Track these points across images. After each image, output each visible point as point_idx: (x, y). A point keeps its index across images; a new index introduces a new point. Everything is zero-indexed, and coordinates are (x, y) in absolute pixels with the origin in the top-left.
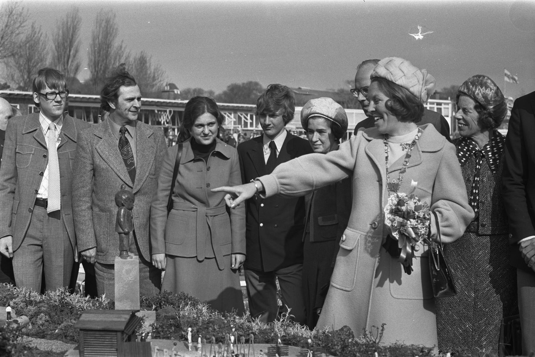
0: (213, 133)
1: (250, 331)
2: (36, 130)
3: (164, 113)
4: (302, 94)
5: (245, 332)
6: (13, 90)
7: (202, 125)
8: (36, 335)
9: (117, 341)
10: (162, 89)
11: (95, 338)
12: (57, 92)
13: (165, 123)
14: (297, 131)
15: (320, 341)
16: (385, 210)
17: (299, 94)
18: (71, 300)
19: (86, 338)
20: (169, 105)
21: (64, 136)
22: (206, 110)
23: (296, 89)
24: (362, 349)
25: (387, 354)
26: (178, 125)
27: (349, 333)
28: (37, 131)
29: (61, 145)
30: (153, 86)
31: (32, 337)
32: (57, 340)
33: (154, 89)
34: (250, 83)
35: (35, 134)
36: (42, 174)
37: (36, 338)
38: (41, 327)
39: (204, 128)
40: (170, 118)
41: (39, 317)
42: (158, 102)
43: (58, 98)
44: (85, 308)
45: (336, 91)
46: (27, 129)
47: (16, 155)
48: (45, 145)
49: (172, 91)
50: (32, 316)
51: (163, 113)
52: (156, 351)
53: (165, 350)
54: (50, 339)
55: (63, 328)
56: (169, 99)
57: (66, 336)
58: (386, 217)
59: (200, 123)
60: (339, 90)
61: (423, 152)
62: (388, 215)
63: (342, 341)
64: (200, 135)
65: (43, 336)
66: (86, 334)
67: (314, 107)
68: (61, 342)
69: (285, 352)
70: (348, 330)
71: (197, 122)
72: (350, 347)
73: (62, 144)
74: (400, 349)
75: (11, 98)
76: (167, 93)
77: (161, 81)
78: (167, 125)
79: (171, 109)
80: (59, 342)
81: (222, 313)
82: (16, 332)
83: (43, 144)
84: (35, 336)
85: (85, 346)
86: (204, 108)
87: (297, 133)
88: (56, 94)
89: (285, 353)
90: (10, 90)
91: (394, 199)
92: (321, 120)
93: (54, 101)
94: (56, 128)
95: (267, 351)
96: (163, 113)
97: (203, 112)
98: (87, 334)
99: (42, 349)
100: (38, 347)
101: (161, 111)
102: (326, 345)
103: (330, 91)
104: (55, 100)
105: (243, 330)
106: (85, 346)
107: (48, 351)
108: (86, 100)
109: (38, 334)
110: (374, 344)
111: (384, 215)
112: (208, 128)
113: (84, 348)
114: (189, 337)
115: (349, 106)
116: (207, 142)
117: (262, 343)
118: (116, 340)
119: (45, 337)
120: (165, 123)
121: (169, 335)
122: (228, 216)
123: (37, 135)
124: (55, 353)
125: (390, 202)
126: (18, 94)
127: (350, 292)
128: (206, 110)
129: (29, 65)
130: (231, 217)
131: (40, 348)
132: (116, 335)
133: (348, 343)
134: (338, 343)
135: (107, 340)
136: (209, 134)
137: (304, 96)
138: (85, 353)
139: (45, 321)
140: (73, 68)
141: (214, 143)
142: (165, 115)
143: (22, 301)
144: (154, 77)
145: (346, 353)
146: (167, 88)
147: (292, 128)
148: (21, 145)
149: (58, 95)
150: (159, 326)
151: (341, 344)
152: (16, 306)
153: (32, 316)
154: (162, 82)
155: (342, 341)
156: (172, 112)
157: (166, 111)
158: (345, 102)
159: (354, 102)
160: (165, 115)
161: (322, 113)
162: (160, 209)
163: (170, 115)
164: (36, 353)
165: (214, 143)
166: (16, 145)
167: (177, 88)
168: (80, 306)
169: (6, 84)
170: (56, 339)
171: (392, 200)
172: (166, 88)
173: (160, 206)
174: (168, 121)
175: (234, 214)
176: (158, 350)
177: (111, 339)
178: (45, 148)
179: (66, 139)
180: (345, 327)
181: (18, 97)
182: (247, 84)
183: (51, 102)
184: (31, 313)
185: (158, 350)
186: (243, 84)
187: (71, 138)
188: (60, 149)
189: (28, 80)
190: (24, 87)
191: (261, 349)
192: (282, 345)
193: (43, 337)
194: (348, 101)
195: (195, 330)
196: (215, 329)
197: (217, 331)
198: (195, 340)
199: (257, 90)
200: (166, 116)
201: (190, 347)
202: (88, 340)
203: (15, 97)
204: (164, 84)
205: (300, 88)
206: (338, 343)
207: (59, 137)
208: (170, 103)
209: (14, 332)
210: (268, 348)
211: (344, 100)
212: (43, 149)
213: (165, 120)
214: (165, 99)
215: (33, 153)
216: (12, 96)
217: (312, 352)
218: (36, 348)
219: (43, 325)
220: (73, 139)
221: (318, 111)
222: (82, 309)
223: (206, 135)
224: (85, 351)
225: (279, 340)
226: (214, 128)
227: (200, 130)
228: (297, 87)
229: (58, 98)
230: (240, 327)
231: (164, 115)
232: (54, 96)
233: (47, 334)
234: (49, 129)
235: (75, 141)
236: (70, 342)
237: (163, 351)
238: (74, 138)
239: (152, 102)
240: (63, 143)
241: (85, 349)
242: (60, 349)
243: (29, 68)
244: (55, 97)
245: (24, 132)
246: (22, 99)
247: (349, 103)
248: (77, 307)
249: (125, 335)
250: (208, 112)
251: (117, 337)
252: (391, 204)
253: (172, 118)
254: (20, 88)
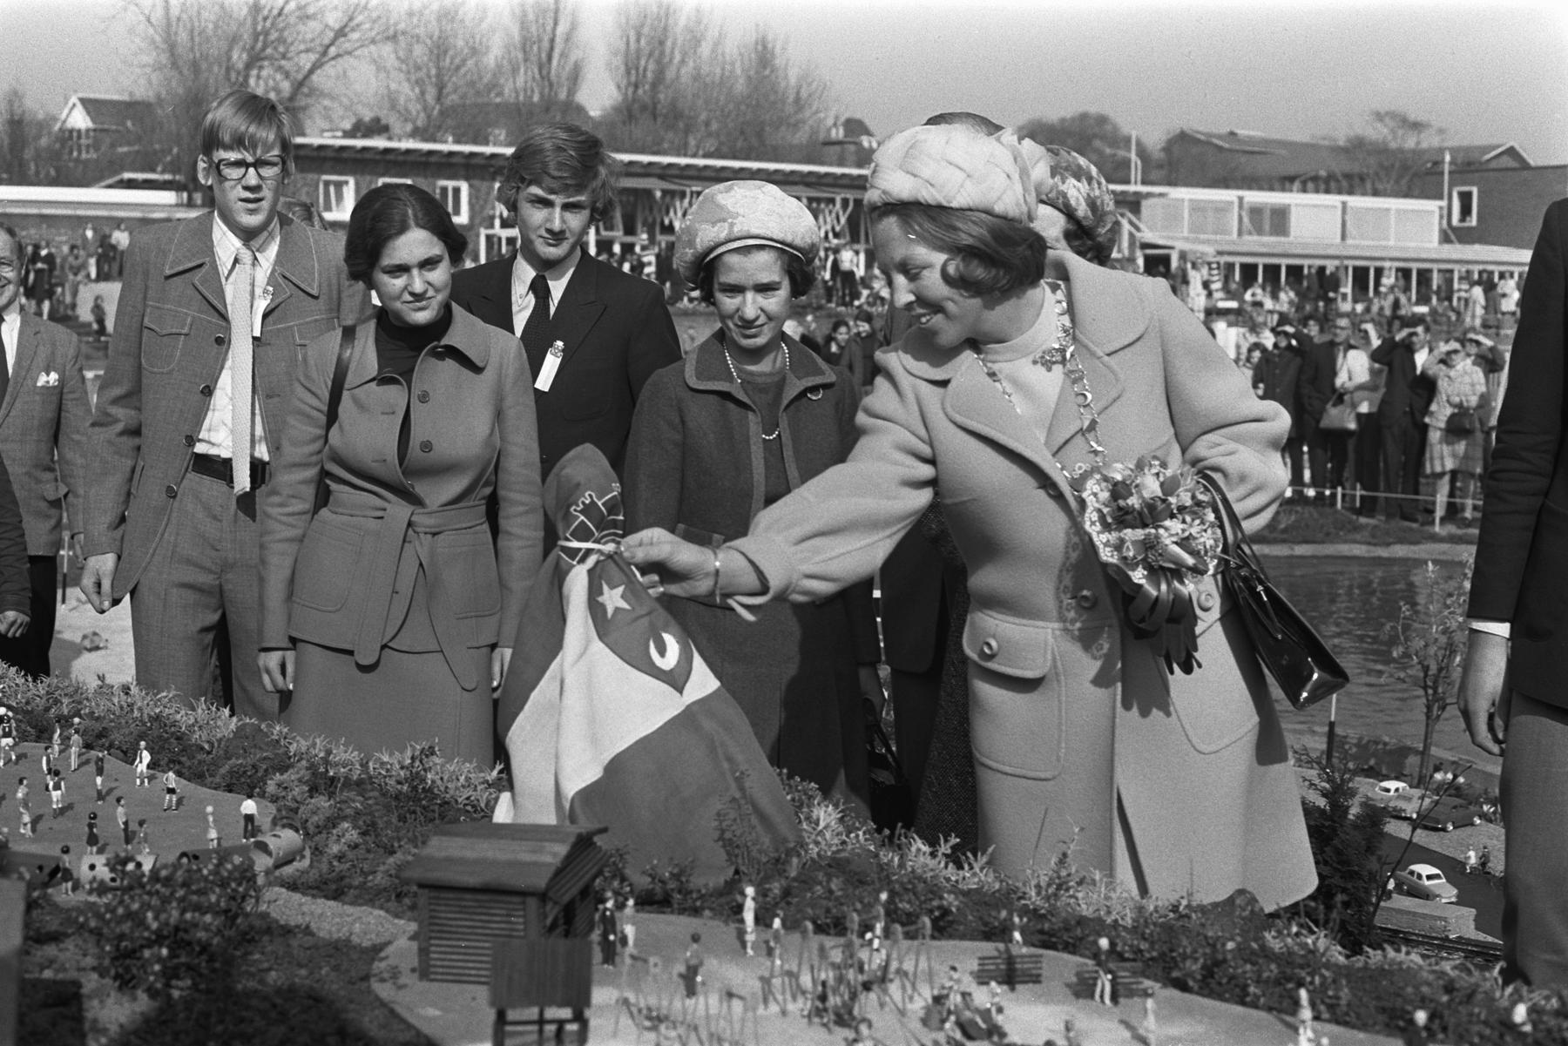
0: (437, 290)
1: (935, 903)
2: (200, 266)
3: (827, 205)
4: (1237, 151)
5: (921, 903)
6: (400, 140)
7: (403, 269)
8: (317, 888)
9: (524, 923)
10: (822, 137)
11: (460, 912)
12: (250, 159)
13: (831, 235)
14: (1218, 263)
15: (1145, 939)
16: (1087, 526)
17: (1230, 150)
18: (442, 779)
19: (434, 910)
20: (825, 181)
21: (280, 280)
22: (412, 223)
23: (1220, 137)
24: (1265, 975)
25: (1342, 994)
26: (867, 241)
27: (1252, 911)
28: (204, 270)
29: (273, 306)
30: (796, 126)
31: (304, 894)
32: (373, 906)
33: (801, 137)
34: (1084, 117)
35: (197, 277)
36: (208, 392)
37: (314, 896)
38: (335, 863)
39: (411, 277)
40: (843, 220)
41: (335, 831)
42: (810, 173)
43: (252, 178)
44: (483, 805)
45: (1341, 143)
46: (174, 263)
47: (141, 331)
48: (223, 311)
49: (850, 143)
50: (318, 827)
51: (823, 206)
52: (628, 961)
53: (652, 960)
54: (352, 904)
55: (393, 872)
56: (841, 164)
57: (399, 896)
58: (1098, 543)
59: (397, 262)
60: (1349, 140)
61: (1108, 355)
62: (1101, 538)
63: (1209, 944)
64: (399, 297)
65: (336, 890)
66: (434, 898)
67: (740, 218)
68: (382, 913)
69: (1034, 972)
70: (1247, 905)
71: (387, 260)
72: (1232, 964)
73: (277, 301)
74: (1391, 972)
75: (389, 162)
76: (837, 148)
77: (817, 112)
78: (835, 241)
79: (848, 196)
80: (377, 912)
81: (887, 832)
82: (240, 884)
83: (220, 307)
84: (315, 892)
85: (433, 935)
86: (405, 215)
87: (1218, 268)
88: (248, 166)
89: (1031, 975)
90: (390, 139)
91: (1096, 489)
92: (764, 257)
93: (239, 187)
94: (256, 258)
95: (975, 967)
96: (823, 206)
97: (403, 229)
98: (438, 898)
99: (321, 934)
100: (313, 926)
101: (818, 200)
102: (1163, 955)
103: (1322, 142)
104: (244, 182)
105: (918, 898)
106: (433, 935)
107: (338, 940)
108: (639, 170)
109: (325, 883)
110: (1310, 956)
111: (1091, 539)
112: (420, 274)
113: (431, 938)
114: (749, 916)
115: (1380, 187)
116: (422, 317)
117: (970, 939)
118: (521, 920)
119: (343, 893)
120: (831, 235)
121: (698, 903)
122: (489, 535)
123: (204, 281)
124: (355, 947)
125: (1091, 502)
126: (408, 151)
127: (1052, 783)
128: (412, 223)
129: (438, 68)
130: (500, 543)
131: (319, 928)
132: (524, 903)
133: (1225, 952)
134: (1195, 951)
135: (498, 919)
136: (426, 292)
137: (1243, 159)
138: (433, 956)
139: (349, 846)
140: (564, 75)
141: (443, 322)
142: (830, 212)
143: (300, 780)
144: (797, 99)
145: (1220, 984)
146: (838, 133)
147: (1202, 253)
148: (158, 308)
149: (251, 170)
150: (671, 873)
151: (1205, 954)
152: (284, 794)
153: (318, 827)
154: (822, 115)
155: (1209, 944)
156: (851, 204)
157: (832, 201)
158: (1368, 175)
159: (1394, 175)
160: (830, 212)
161: (769, 234)
162: (284, 519)
163: (844, 211)
164: (300, 946)
165: (443, 322)
166: (145, 306)
167: (869, 133)
168: (468, 798)
169: (377, 120)
170: (371, 902)
171: (1095, 495)
172: (834, 132)
173: (280, 510)
174: (838, 229)
175: (509, 533)
176: (633, 957)
177: (508, 915)
178: (224, 317)
179: (288, 290)
180: (1241, 892)
181: (410, 158)
182: (1073, 119)
183: (233, 187)
184: (316, 818)
185: (633, 957)
186: (1063, 120)
187: (302, 286)
188: (270, 318)
189: (438, 107)
190: (425, 130)
191: (951, 963)
192: (1025, 950)
193: (337, 895)
194: (1377, 174)
195: (776, 891)
196: (831, 892)
197: (837, 899)
198: (762, 920)
199: (1103, 138)
200: (834, 215)
201: (749, 945)
202: (443, 915)
203: (401, 158)
204: (830, 122)
205: (1232, 134)
206: (1195, 951)
207: (268, 284)
208: (844, 175)
209: (233, 885)
210: (980, 959)
211: (1365, 170)
212: (215, 320)
213: (829, 227)
214: (831, 164)
215: (185, 331)
216: (391, 157)
217: (1109, 977)
218: (307, 931)
219: (340, 857)
220: (309, 290)
221: (755, 231)
222: (473, 806)
223: (418, 297)
224: (433, 949)
225: (1017, 936)
226: (440, 275)
227: (399, 282)
228: (1224, 130)
229: (252, 178)
230: (906, 890)
231: (827, 212)
232: (243, 170)
233: (350, 887)
234: (236, 261)
235: (315, 292)
236: (409, 914)
237: (646, 961)
238: (309, 285)
239: (792, 172)
240: (280, 300)
241: (433, 942)
242: (373, 936)
243: (438, 76)
244: (244, 175)
245: (168, 272)
246: (421, 163)
247: (1380, 180)
248: (460, 800)
249: (549, 906)
250: (419, 225)
251: (524, 910)
252: (1097, 505)
253: (849, 220)
254: (416, 133)
